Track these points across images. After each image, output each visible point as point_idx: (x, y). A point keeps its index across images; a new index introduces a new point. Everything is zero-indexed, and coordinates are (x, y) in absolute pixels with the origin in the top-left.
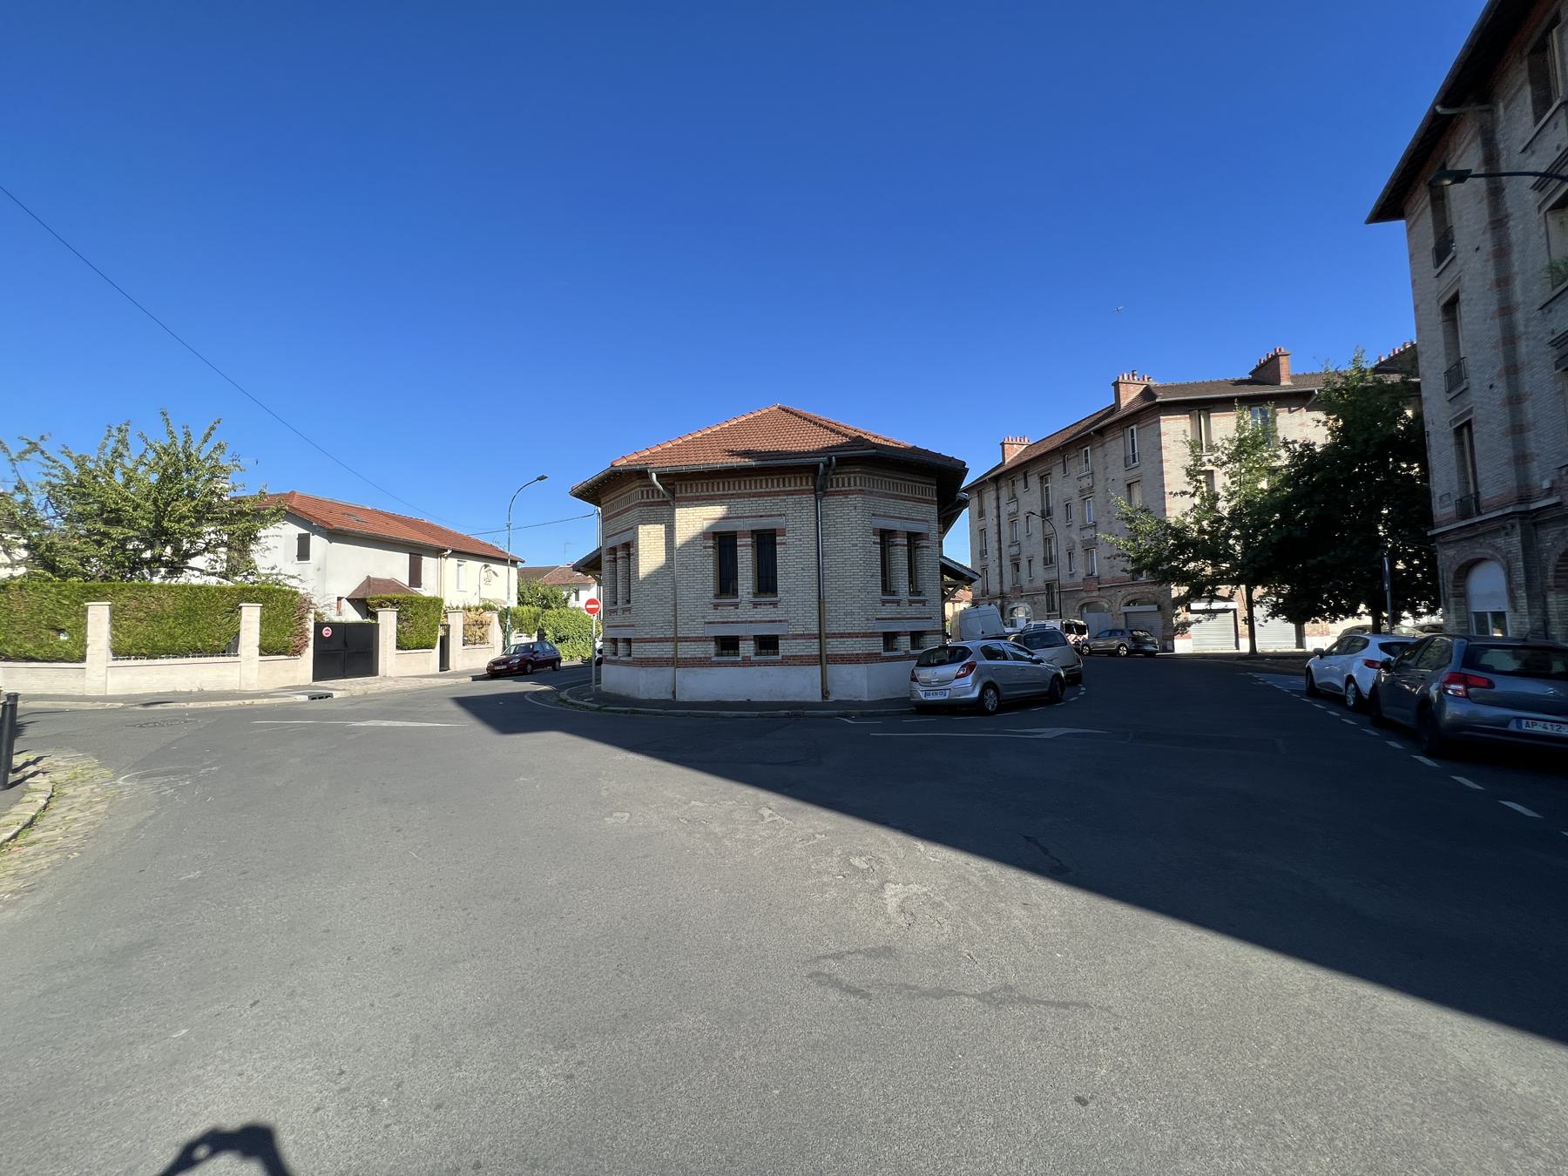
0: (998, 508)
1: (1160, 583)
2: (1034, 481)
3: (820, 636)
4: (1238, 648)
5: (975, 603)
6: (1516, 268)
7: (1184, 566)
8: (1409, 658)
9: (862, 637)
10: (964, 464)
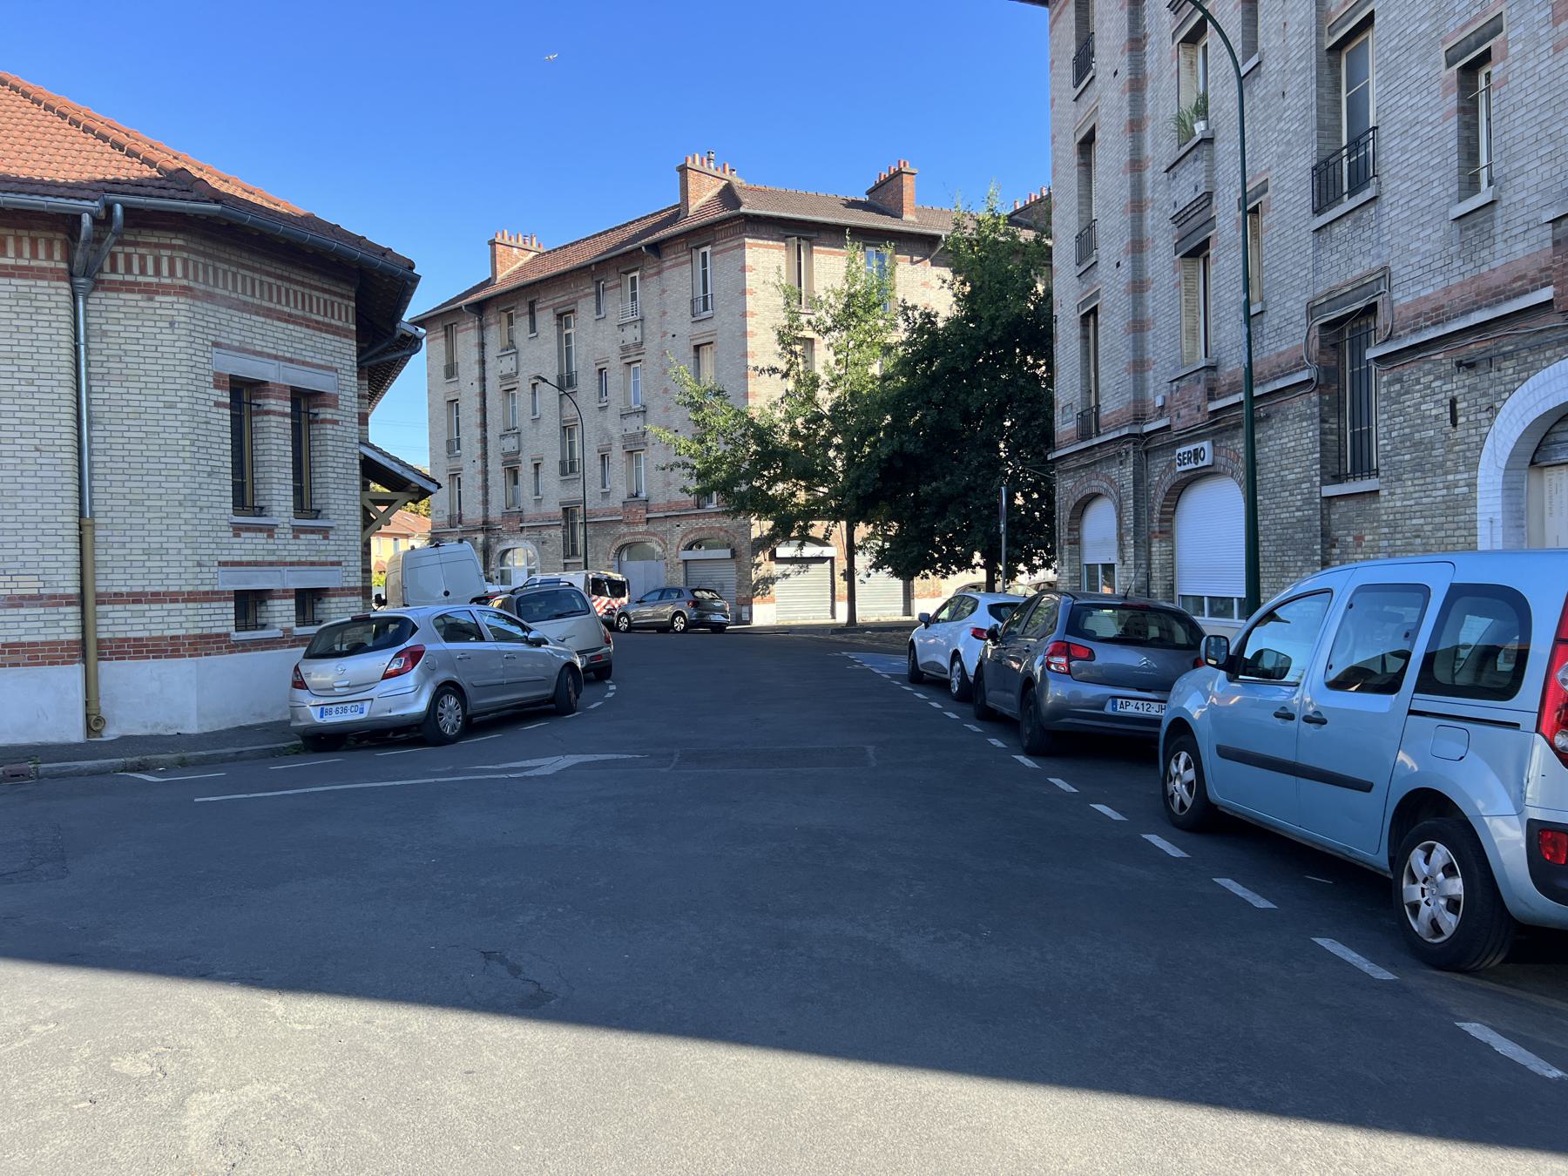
0: (483, 362)
1: (735, 513)
2: (546, 320)
3: (81, 600)
4: (834, 617)
5: (436, 540)
6: (1149, 112)
7: (770, 488)
8: (1018, 623)
9: (184, 601)
10: (411, 266)
